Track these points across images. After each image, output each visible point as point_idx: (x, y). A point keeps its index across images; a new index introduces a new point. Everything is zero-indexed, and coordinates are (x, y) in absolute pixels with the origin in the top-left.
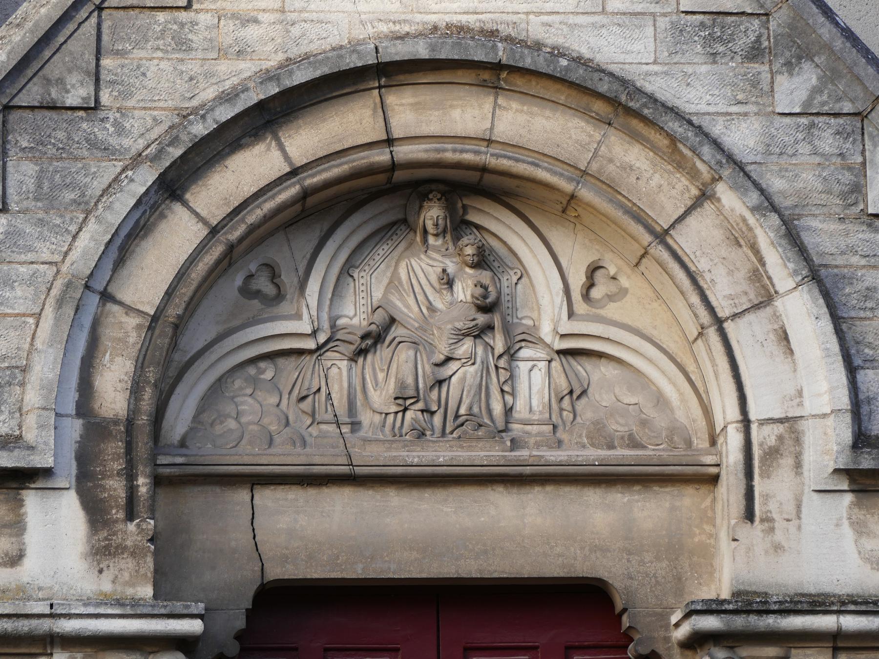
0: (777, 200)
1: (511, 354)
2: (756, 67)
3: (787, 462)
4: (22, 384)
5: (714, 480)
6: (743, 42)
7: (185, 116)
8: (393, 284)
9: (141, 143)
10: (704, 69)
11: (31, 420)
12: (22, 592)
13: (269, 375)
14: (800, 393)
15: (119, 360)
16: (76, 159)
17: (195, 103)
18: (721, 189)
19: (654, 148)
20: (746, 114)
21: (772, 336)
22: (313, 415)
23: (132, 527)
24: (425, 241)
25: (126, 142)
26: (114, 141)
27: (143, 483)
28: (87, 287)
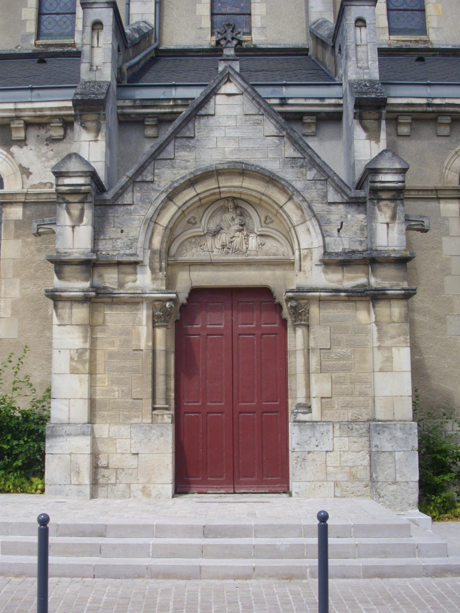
0: (307, 199)
1: (248, 235)
2: (302, 169)
3: (309, 258)
4: (137, 242)
5: (293, 263)
6: (299, 164)
7: (173, 182)
8: (221, 220)
9: (163, 189)
10: (290, 170)
11: (138, 250)
12: (137, 288)
13: (193, 240)
14: (312, 243)
15: (158, 237)
16: (149, 192)
17: (175, 180)
18: (294, 197)
19: (279, 187)
20: (300, 180)
21: (306, 230)
22: (203, 250)
23: (161, 273)
24: (228, 210)
25: (160, 189)
26: (158, 188)
27: (163, 264)
28: (151, 220)
